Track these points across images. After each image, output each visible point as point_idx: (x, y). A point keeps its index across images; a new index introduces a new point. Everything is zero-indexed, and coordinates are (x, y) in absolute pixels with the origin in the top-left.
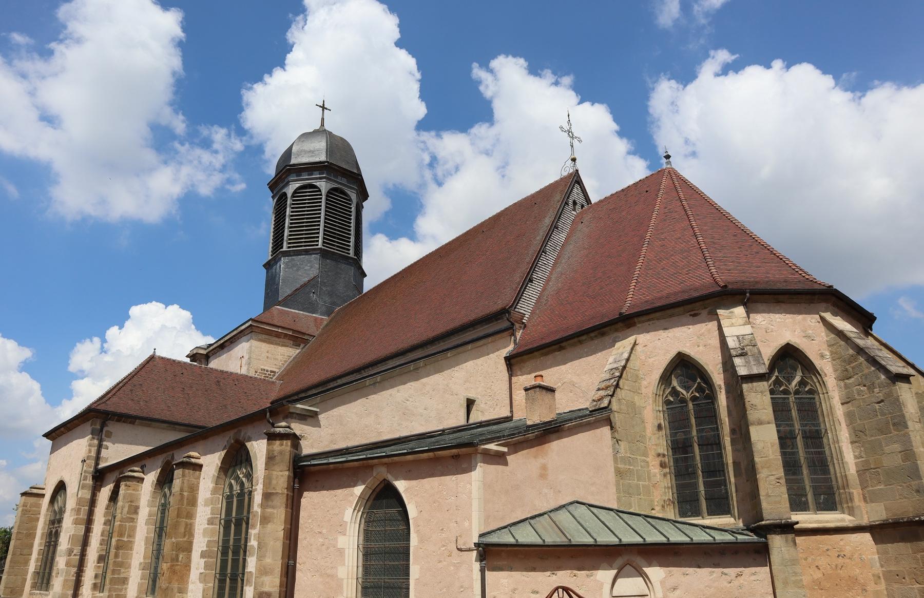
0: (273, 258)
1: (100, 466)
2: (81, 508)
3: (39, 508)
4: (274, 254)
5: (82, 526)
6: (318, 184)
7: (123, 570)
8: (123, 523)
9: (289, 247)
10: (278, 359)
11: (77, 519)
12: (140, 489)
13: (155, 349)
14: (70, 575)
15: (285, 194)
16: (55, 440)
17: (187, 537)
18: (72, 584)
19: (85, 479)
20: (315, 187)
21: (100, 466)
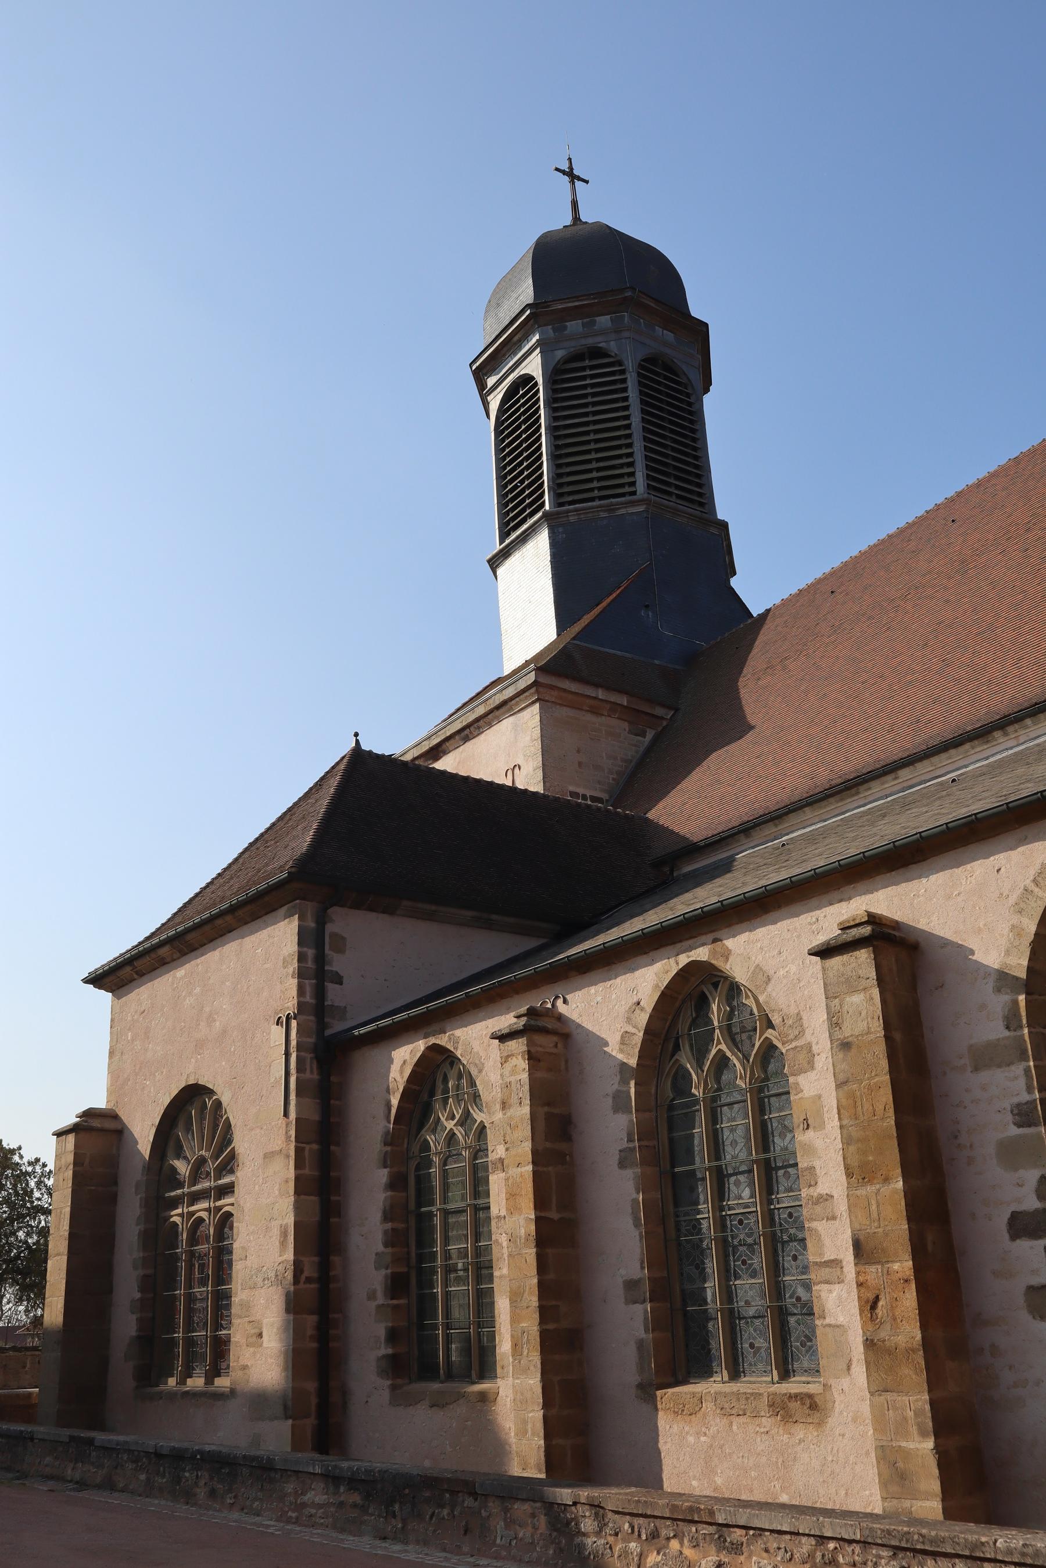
0: (558, 513)
1: (328, 1032)
6: (613, 347)
13: (356, 735)
20: (604, 354)
21: (328, 1032)
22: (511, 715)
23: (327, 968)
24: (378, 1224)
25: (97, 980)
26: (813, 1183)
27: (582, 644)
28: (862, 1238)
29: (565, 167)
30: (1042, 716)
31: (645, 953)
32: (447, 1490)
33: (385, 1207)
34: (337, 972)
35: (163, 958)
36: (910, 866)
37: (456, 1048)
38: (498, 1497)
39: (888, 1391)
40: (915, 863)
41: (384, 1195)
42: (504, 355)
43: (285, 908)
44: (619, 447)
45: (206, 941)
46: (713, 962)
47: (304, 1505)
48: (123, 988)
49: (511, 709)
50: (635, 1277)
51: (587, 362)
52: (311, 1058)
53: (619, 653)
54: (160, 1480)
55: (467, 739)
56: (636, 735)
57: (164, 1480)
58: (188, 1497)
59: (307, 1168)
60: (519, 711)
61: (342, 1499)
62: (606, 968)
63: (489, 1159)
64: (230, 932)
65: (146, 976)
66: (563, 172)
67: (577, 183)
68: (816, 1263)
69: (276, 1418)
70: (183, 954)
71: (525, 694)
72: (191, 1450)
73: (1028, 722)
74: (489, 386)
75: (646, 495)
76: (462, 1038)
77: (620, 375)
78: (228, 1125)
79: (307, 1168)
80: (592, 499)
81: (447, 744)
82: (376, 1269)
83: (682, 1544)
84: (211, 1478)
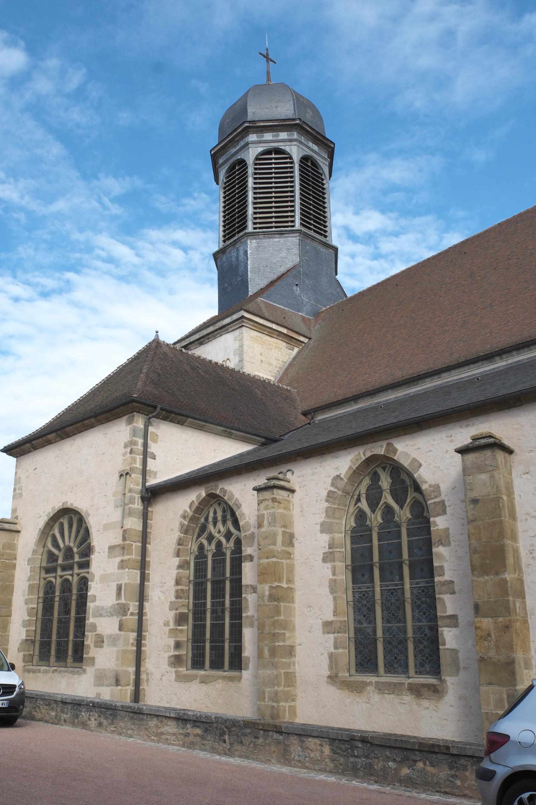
1: (148, 484)
2: (132, 545)
3: (14, 550)
4: (229, 239)
5: (136, 571)
6: (287, 149)
7: (287, 635)
8: (279, 560)
9: (255, 228)
10: (272, 365)
11: (122, 561)
12: (291, 508)
13: (157, 332)
14: (128, 645)
15: (242, 163)
16: (18, 458)
17: (517, 573)
18: (132, 657)
19: (132, 501)
21: (148, 484)
22: (227, 333)
23: (148, 450)
24: (173, 586)
25: (10, 450)
26: (442, 574)
27: (264, 300)
28: (480, 603)
29: (264, 53)
30: (532, 347)
31: (345, 449)
32: (261, 729)
33: (177, 578)
34: (153, 453)
35: (50, 440)
36: (511, 409)
37: (224, 496)
38: (297, 734)
39: (492, 684)
40: (515, 407)
41: (177, 571)
42: (229, 148)
43: (127, 416)
44: (287, 202)
45: (77, 432)
46: (387, 455)
47: (162, 734)
48: (25, 456)
49: (228, 329)
50: (330, 620)
51: (273, 155)
52: (138, 497)
53: (282, 307)
54: (65, 716)
55: (201, 344)
56: (289, 349)
57: (68, 716)
58: (84, 725)
59: (134, 555)
60: (232, 331)
61: (188, 731)
62: (320, 456)
63: (243, 554)
64: (92, 428)
65: (38, 450)
66: (264, 56)
67: (271, 63)
68: (441, 617)
69: (111, 685)
70: (62, 439)
71: (236, 323)
72: (86, 701)
73: (514, 353)
74: (219, 164)
75: (300, 228)
76: (228, 490)
77: (290, 164)
78: (87, 531)
79: (134, 555)
80: (271, 227)
81: (190, 346)
82: (170, 610)
83: (425, 764)
84: (100, 716)
